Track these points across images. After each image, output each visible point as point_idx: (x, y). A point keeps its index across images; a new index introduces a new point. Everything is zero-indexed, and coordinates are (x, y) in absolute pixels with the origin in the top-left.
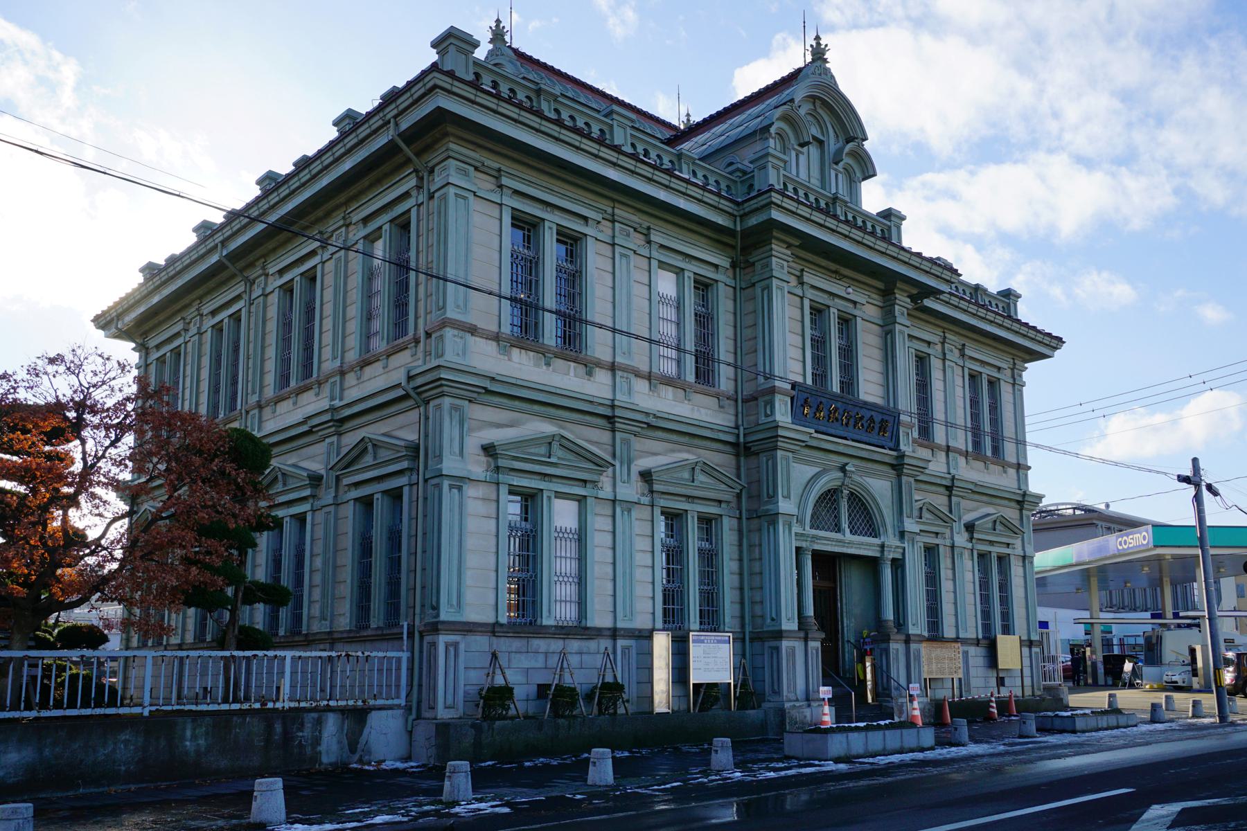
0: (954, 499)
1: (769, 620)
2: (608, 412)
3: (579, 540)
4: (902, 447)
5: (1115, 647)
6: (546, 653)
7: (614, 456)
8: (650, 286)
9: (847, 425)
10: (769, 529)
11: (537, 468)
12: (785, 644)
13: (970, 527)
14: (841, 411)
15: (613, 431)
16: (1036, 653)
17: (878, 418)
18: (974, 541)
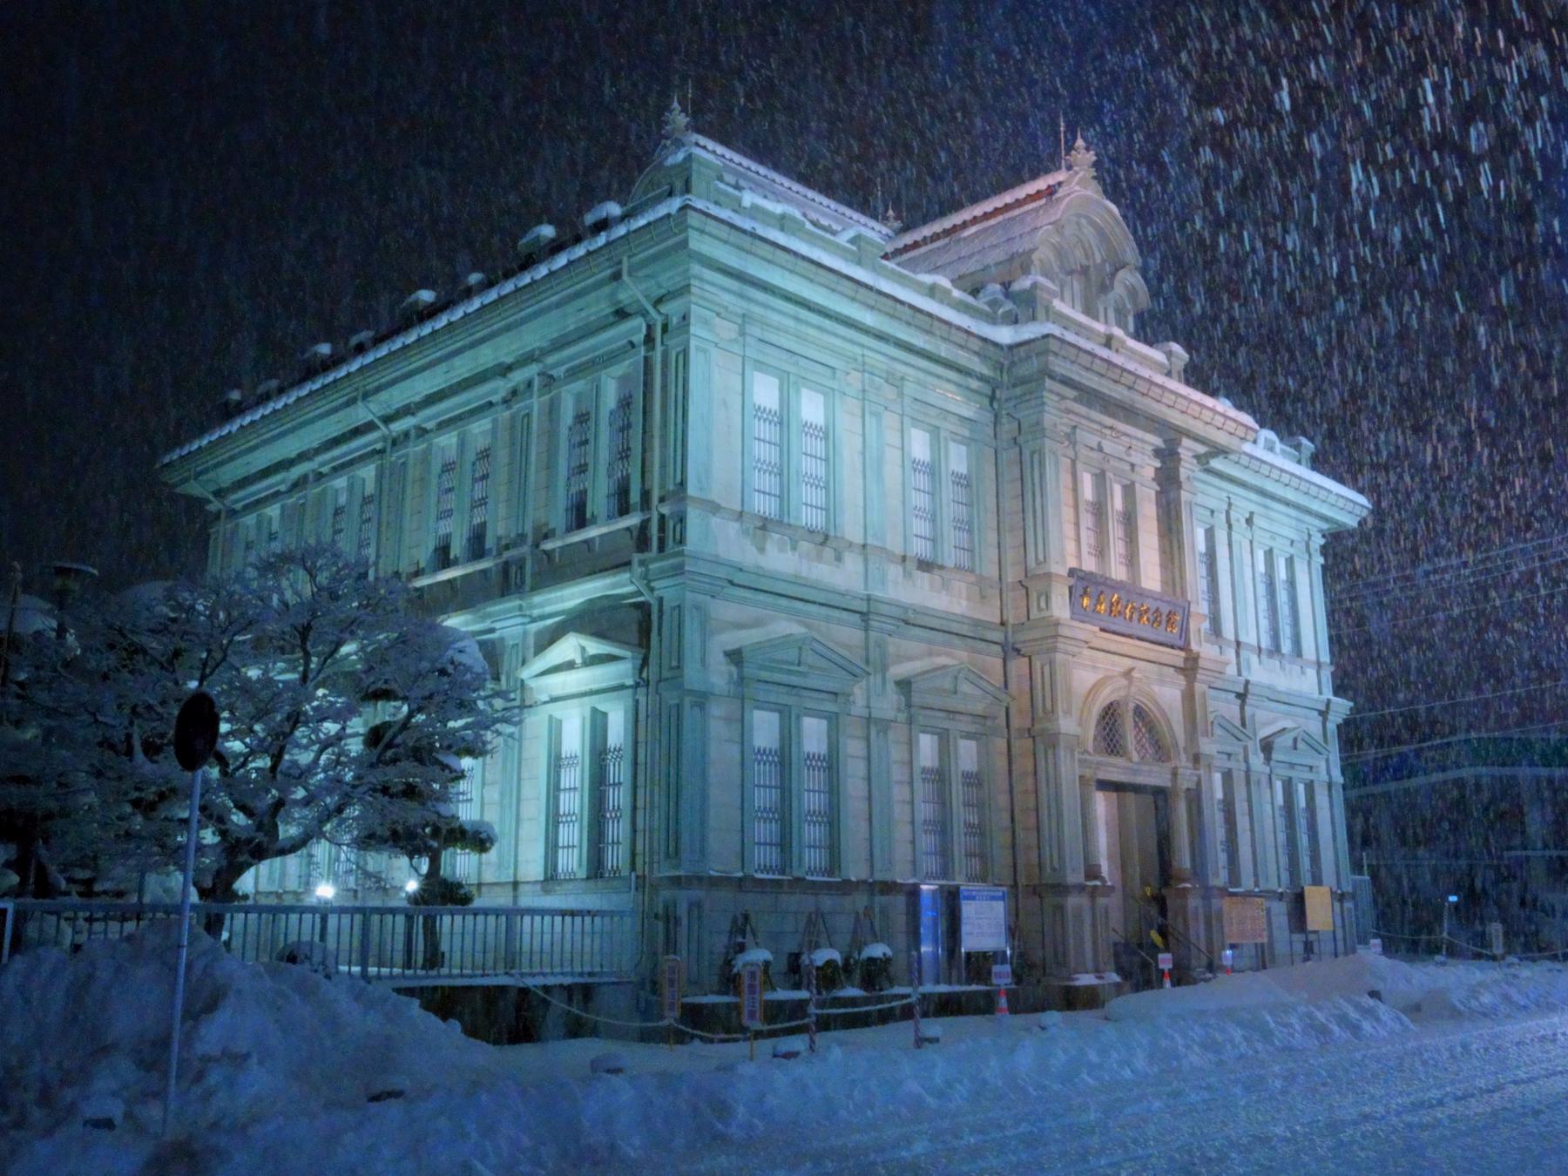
0: (1247, 709)
1: (1049, 870)
2: (863, 607)
3: (781, 763)
4: (1194, 647)
5: (376, 969)
6: (796, 913)
7: (867, 662)
8: (903, 449)
9: (1131, 618)
10: (1046, 751)
11: (784, 678)
12: (1072, 901)
13: (1267, 747)
14: (1123, 602)
15: (866, 630)
16: (1349, 910)
17: (1165, 610)
18: (1272, 763)
